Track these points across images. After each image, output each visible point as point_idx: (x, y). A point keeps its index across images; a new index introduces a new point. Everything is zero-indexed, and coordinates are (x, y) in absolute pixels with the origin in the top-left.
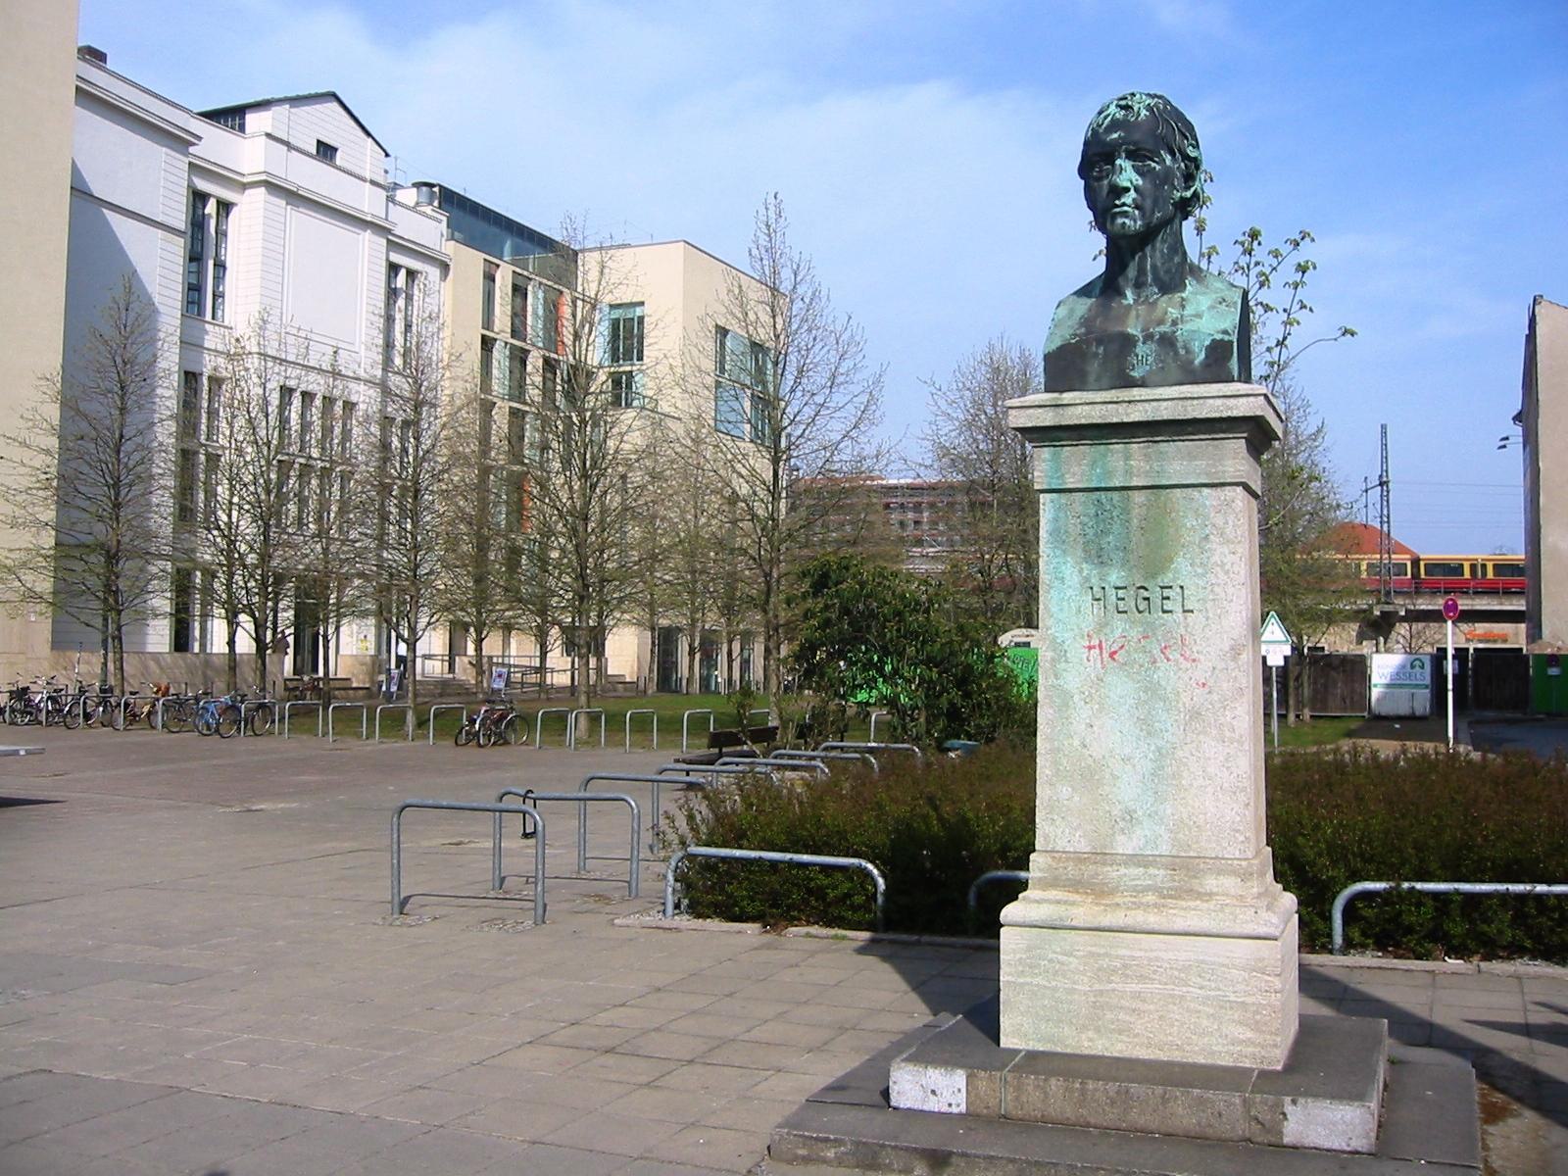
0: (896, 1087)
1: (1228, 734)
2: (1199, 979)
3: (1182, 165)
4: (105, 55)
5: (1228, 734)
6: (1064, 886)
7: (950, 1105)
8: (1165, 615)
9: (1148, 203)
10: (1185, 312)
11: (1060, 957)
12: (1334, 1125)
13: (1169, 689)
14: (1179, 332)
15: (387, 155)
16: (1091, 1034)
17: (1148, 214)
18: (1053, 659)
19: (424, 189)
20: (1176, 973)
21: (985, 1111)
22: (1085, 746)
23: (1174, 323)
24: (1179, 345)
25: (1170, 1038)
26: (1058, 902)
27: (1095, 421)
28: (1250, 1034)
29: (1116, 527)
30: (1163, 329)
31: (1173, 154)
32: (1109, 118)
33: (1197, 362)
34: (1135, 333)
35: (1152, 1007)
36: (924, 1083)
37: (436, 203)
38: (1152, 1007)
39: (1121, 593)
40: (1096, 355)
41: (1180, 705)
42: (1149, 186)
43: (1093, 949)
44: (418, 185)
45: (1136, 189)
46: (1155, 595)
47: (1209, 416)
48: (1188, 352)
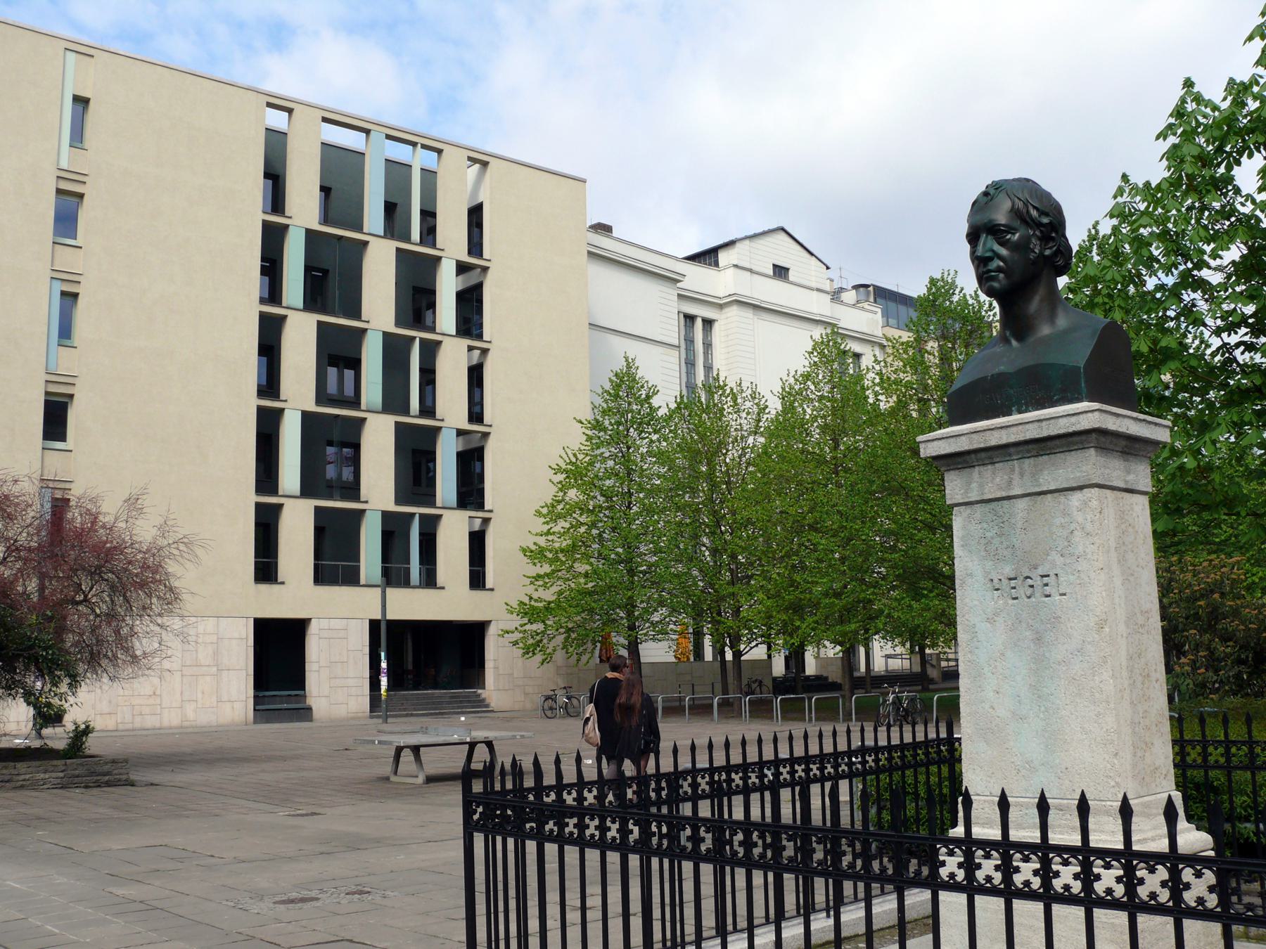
1: (1097, 695)
4: (611, 227)
15: (828, 268)
19: (861, 289)
37: (872, 299)
39: (1013, 583)
44: (856, 287)
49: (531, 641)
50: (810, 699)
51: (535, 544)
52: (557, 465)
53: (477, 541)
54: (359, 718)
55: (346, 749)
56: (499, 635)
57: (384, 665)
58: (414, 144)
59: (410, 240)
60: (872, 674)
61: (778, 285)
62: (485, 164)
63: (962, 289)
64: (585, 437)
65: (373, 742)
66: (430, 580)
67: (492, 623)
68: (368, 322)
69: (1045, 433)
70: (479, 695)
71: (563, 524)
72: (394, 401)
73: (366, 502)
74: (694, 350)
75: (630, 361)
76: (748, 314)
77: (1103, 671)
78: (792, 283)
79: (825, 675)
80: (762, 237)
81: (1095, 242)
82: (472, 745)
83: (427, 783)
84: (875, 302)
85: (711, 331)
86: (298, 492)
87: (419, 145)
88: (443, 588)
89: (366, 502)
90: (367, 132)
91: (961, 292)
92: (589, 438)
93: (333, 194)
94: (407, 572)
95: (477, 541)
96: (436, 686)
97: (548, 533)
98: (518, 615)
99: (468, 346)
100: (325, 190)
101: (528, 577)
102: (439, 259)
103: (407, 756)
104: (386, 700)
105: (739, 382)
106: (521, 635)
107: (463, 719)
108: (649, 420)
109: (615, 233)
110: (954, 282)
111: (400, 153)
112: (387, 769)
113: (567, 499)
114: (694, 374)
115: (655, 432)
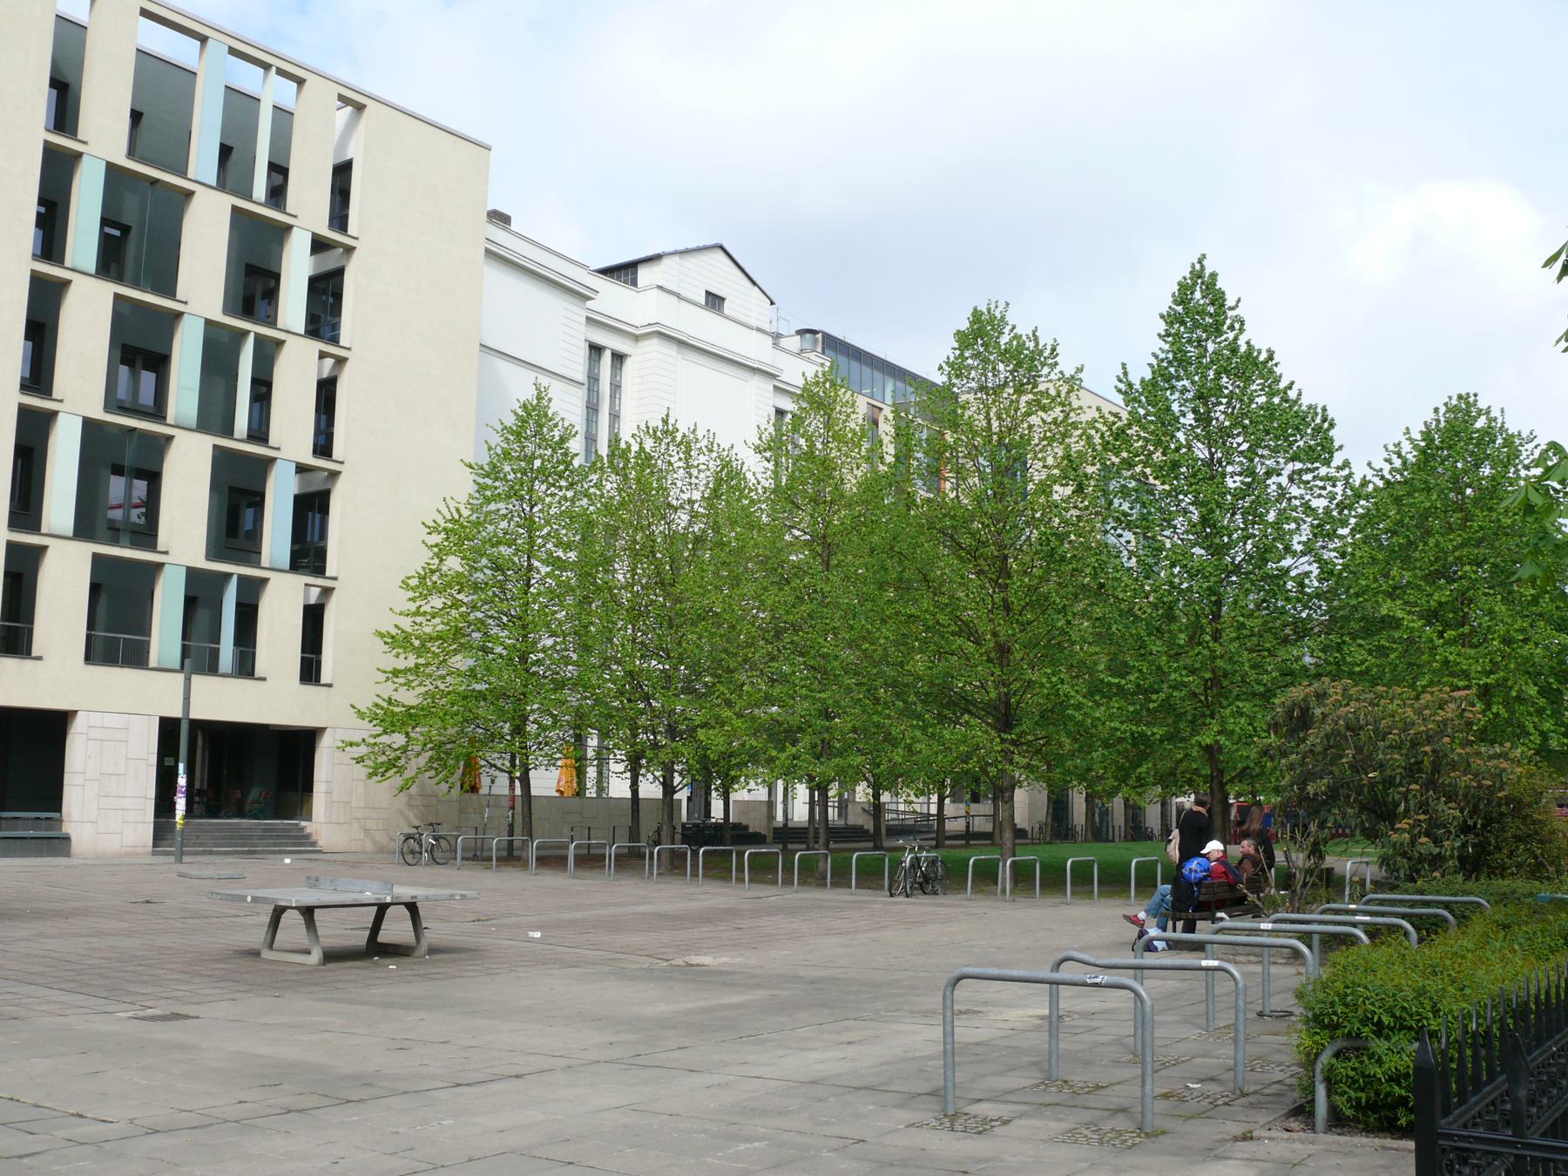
15: (772, 303)
19: (808, 335)
37: (819, 349)
44: (802, 332)
49: (383, 759)
50: (740, 855)
51: (396, 626)
52: (434, 521)
53: (313, 618)
54: (137, 854)
55: (148, 902)
56: (338, 748)
57: (182, 781)
58: (266, 67)
59: (251, 197)
60: (790, 825)
61: (709, 317)
62: (360, 108)
63: (1014, 327)
64: (476, 487)
65: (244, 898)
66: (245, 667)
67: (328, 730)
68: (186, 303)
70: (302, 829)
71: (437, 602)
72: (215, 417)
73: (166, 553)
74: (598, 392)
75: (543, 389)
76: (670, 351)
78: (727, 317)
79: (744, 823)
80: (695, 254)
81: (1199, 281)
82: (382, 908)
83: (324, 964)
84: (823, 353)
85: (621, 369)
86: (70, 533)
87: (274, 69)
88: (264, 679)
89: (166, 553)
90: (203, 40)
91: (1012, 330)
92: (482, 488)
93: (144, 120)
94: (215, 655)
95: (313, 618)
96: (241, 814)
97: (417, 613)
98: (371, 721)
99: (320, 351)
100: (136, 116)
101: (385, 672)
102: (289, 228)
103: (292, 919)
104: (183, 830)
105: (692, 428)
106: (370, 749)
107: (288, 861)
108: (560, 469)
109: (514, 226)
110: (1003, 318)
111: (248, 78)
112: (257, 937)
113: (444, 568)
114: (597, 423)
115: (571, 486)
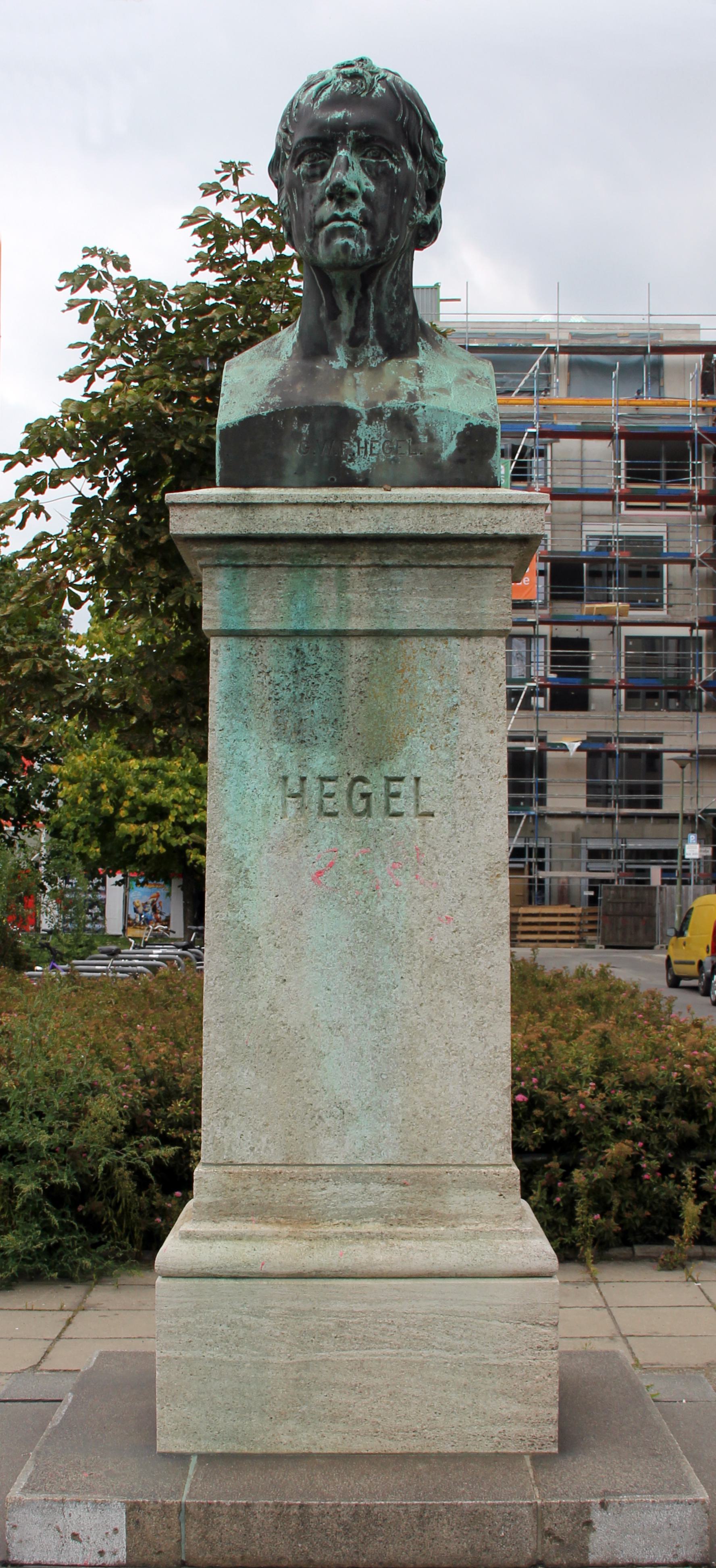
0: (16, 1534)
2: (447, 1338)
3: (425, 173)
5: (481, 989)
6: (246, 1214)
7: (102, 1553)
8: (394, 820)
9: (381, 219)
10: (424, 385)
11: (245, 1318)
12: (657, 1531)
13: (398, 927)
14: (421, 410)
16: (291, 1424)
17: (379, 238)
18: (229, 884)
20: (414, 1331)
21: (156, 1558)
22: (274, 1010)
23: (412, 397)
24: (420, 428)
25: (405, 1422)
26: (239, 1238)
27: (300, 531)
28: (516, 1408)
29: (324, 688)
30: (395, 403)
31: (415, 156)
32: (328, 90)
33: (445, 455)
34: (355, 407)
35: (379, 1381)
36: (60, 1524)
38: (379, 1381)
40: (297, 435)
41: (415, 949)
42: (383, 195)
43: (295, 1304)
45: (366, 197)
46: (376, 787)
47: (467, 531)
48: (432, 439)
69: (440, 529)
77: (495, 948)
